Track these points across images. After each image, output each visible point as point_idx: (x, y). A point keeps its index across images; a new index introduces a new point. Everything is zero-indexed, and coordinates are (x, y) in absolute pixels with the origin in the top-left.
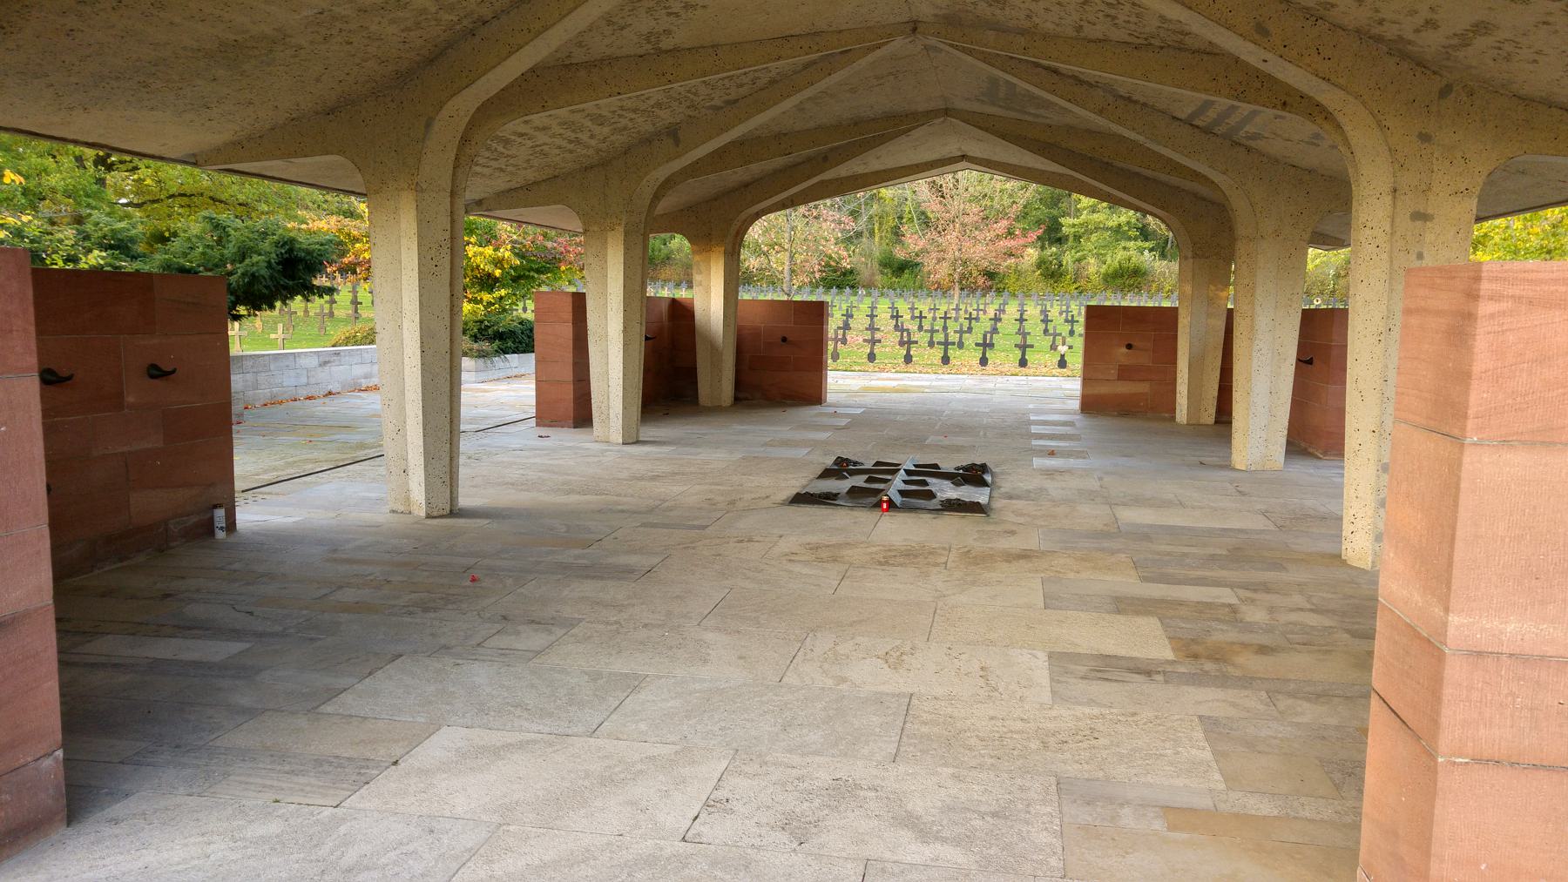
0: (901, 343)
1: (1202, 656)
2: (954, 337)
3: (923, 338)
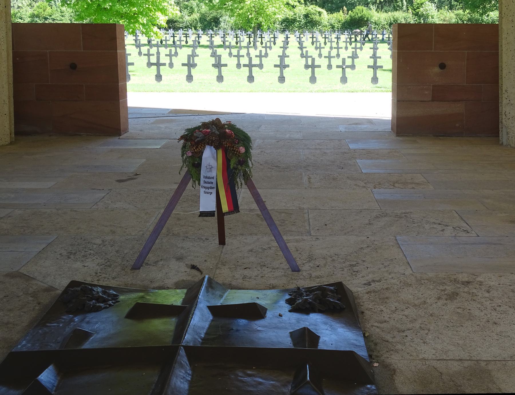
0: (307, 67)
1: (387, 366)
2: (256, 61)
3: (323, 62)
